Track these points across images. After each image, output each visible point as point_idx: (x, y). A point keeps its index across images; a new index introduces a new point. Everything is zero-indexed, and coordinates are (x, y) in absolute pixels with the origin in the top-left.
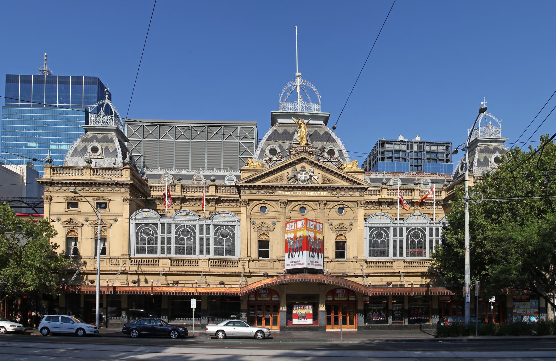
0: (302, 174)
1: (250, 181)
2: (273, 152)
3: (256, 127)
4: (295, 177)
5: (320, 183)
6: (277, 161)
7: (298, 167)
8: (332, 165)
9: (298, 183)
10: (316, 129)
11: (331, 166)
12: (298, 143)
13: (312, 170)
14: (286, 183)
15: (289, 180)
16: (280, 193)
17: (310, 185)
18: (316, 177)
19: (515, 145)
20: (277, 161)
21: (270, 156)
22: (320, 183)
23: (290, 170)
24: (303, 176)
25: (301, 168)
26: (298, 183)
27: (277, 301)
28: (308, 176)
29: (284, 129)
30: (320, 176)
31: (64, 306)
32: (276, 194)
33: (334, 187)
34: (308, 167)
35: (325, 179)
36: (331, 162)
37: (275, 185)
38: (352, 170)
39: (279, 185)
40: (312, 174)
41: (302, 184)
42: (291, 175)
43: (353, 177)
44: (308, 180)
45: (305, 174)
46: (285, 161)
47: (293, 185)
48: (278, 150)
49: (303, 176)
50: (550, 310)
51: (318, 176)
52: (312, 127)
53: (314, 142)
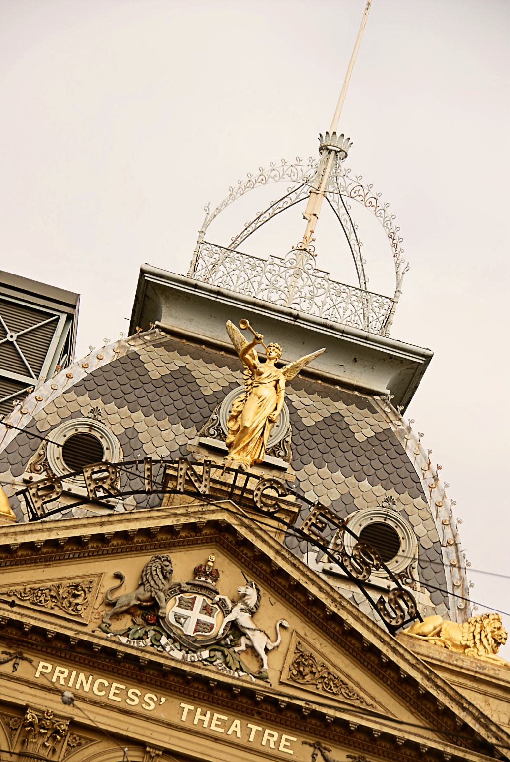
0: (190, 606)
1: (418, 654)
2: (82, 451)
3: (70, 318)
4: (149, 611)
5: (276, 671)
6: (83, 500)
7: (183, 563)
8: (366, 608)
9: (156, 641)
10: (340, 406)
11: (358, 608)
12: (222, 445)
13: (252, 601)
14: (90, 625)
15: (116, 616)
16: (44, 668)
17: (216, 673)
18: (260, 642)
19: (229, 655)
20: (83, 500)
21: (59, 467)
22: (273, 677)
23: (131, 566)
24: (195, 615)
25: (197, 572)
26: (156, 641)
27: (139, 604)
28: (218, 623)
29: (179, 361)
30: (283, 636)
31: (298, 509)
32: (24, 670)
33: (43, 632)
34: (232, 579)
35: (302, 664)
36: (363, 585)
37: (31, 620)
38: (465, 662)
39: (52, 626)
40: (244, 620)
41: (386, 555)
42: (128, 593)
43: (459, 700)
44: (217, 644)
45: (207, 610)
46: (128, 516)
47: (125, 645)
48: (113, 454)
49: (195, 615)
50: (360, 754)
51: (272, 639)
52: (323, 394)
53: (311, 467)
